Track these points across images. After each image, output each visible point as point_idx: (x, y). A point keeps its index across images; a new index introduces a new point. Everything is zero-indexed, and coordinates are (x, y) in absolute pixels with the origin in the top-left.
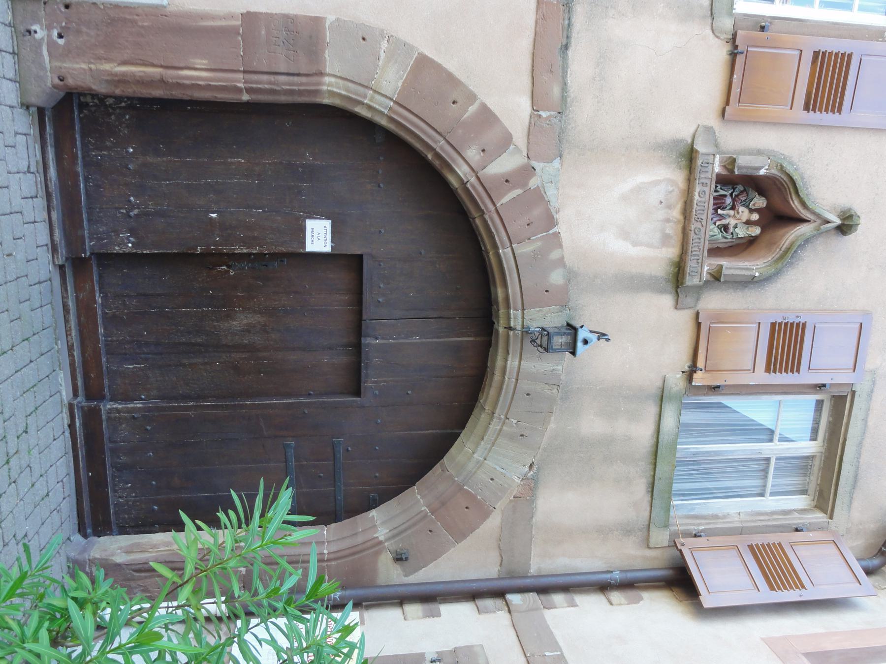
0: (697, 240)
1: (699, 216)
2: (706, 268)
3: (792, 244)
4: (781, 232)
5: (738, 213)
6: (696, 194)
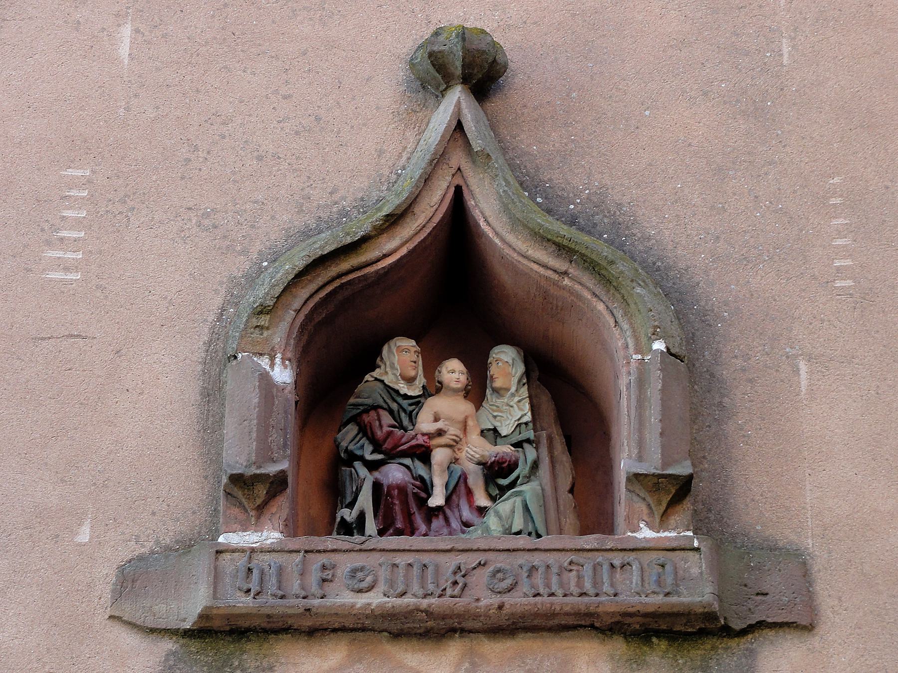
0: (539, 579)
1: (446, 580)
2: (646, 533)
3: (542, 238)
4: (505, 277)
5: (440, 433)
6: (361, 600)
